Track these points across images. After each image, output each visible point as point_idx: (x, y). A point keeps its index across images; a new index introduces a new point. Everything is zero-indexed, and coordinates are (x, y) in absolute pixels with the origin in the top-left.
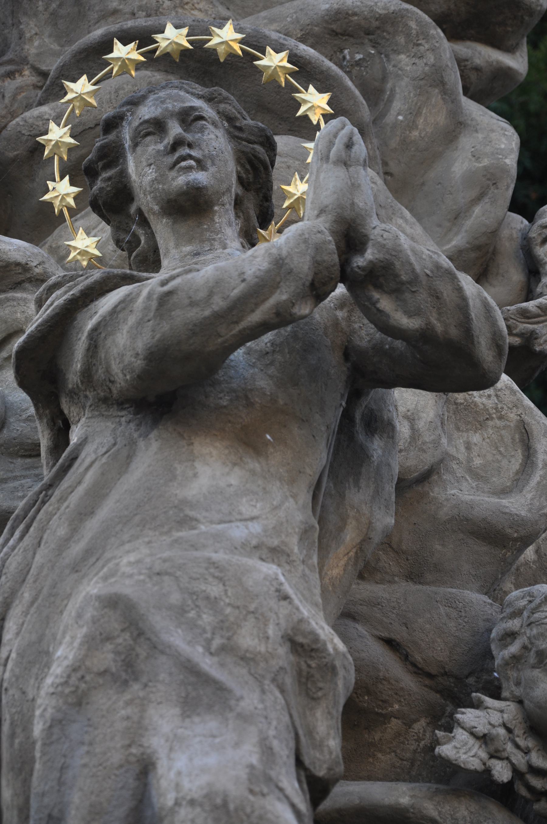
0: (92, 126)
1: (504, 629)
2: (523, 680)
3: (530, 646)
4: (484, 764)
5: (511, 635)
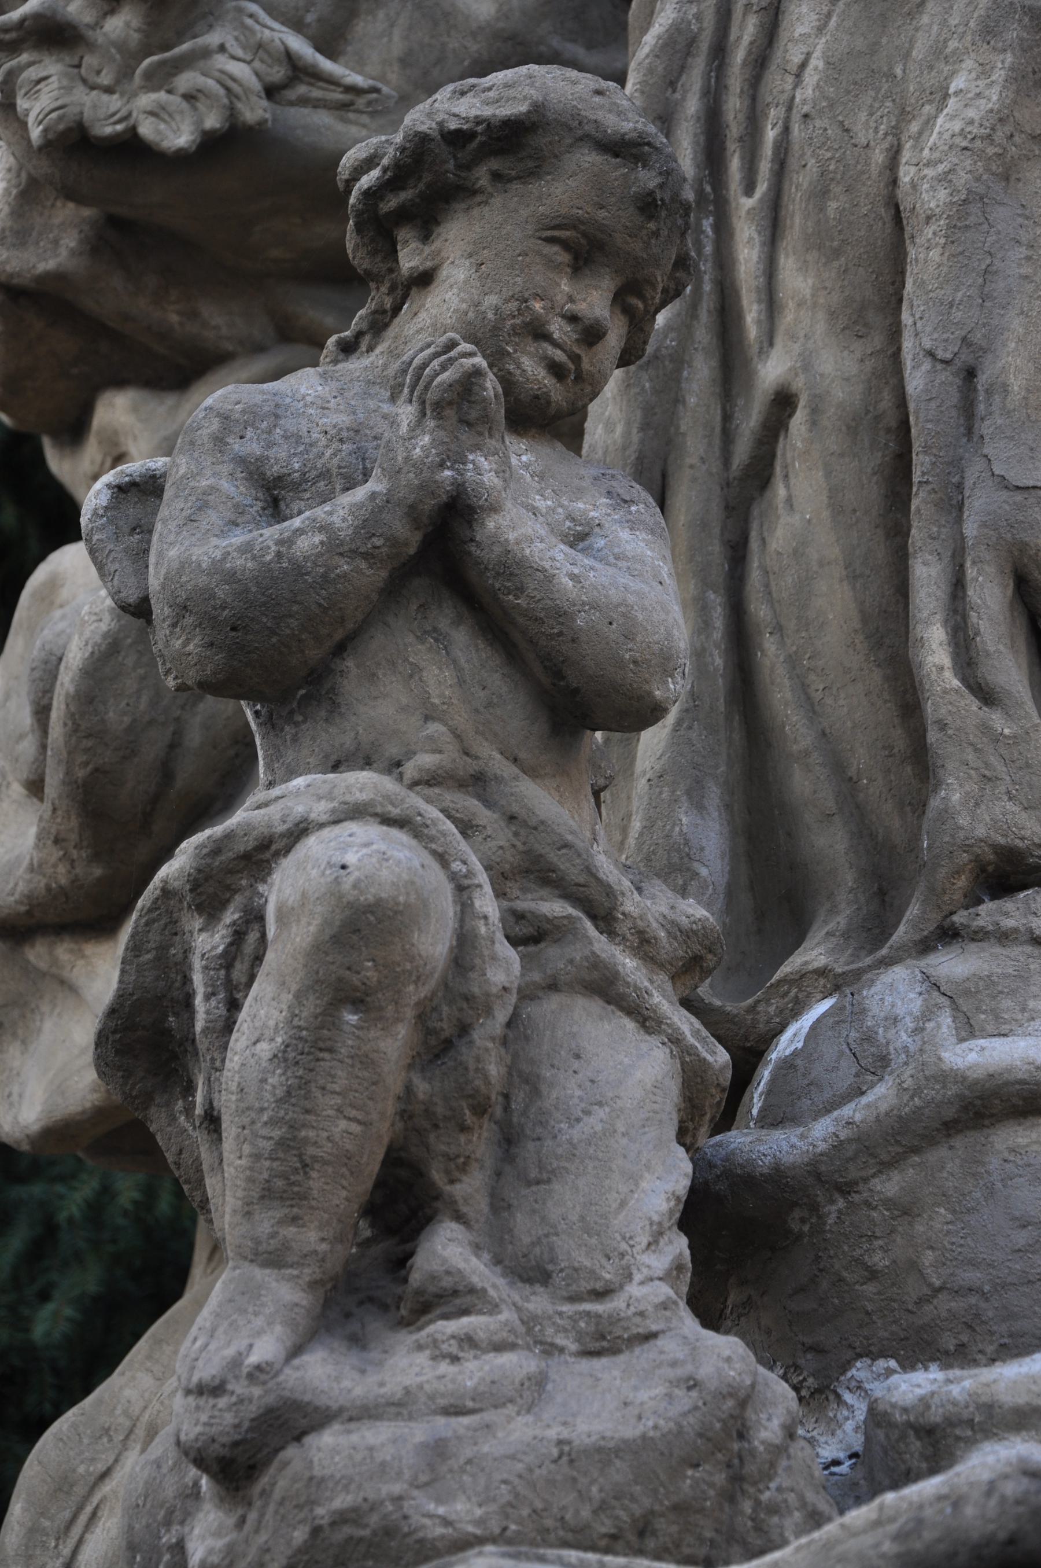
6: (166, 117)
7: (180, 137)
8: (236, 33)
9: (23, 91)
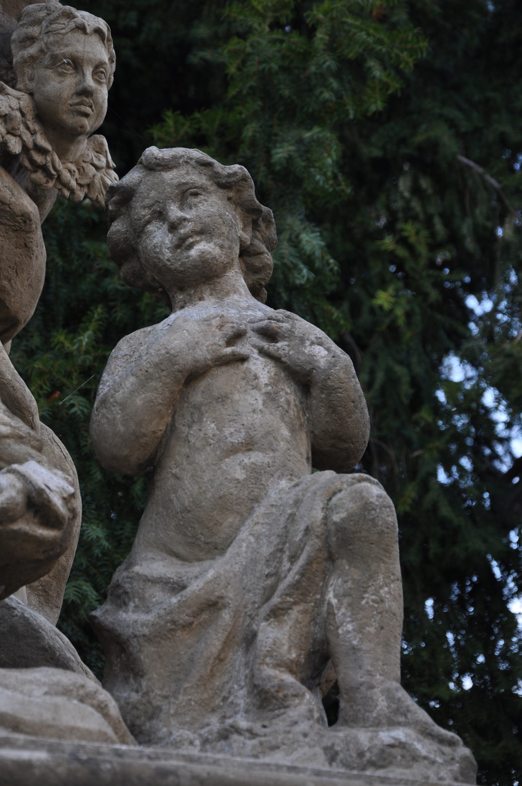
1: (26, 34)
2: (36, 77)
3: (46, 50)
4: (3, 137)
5: (31, 39)
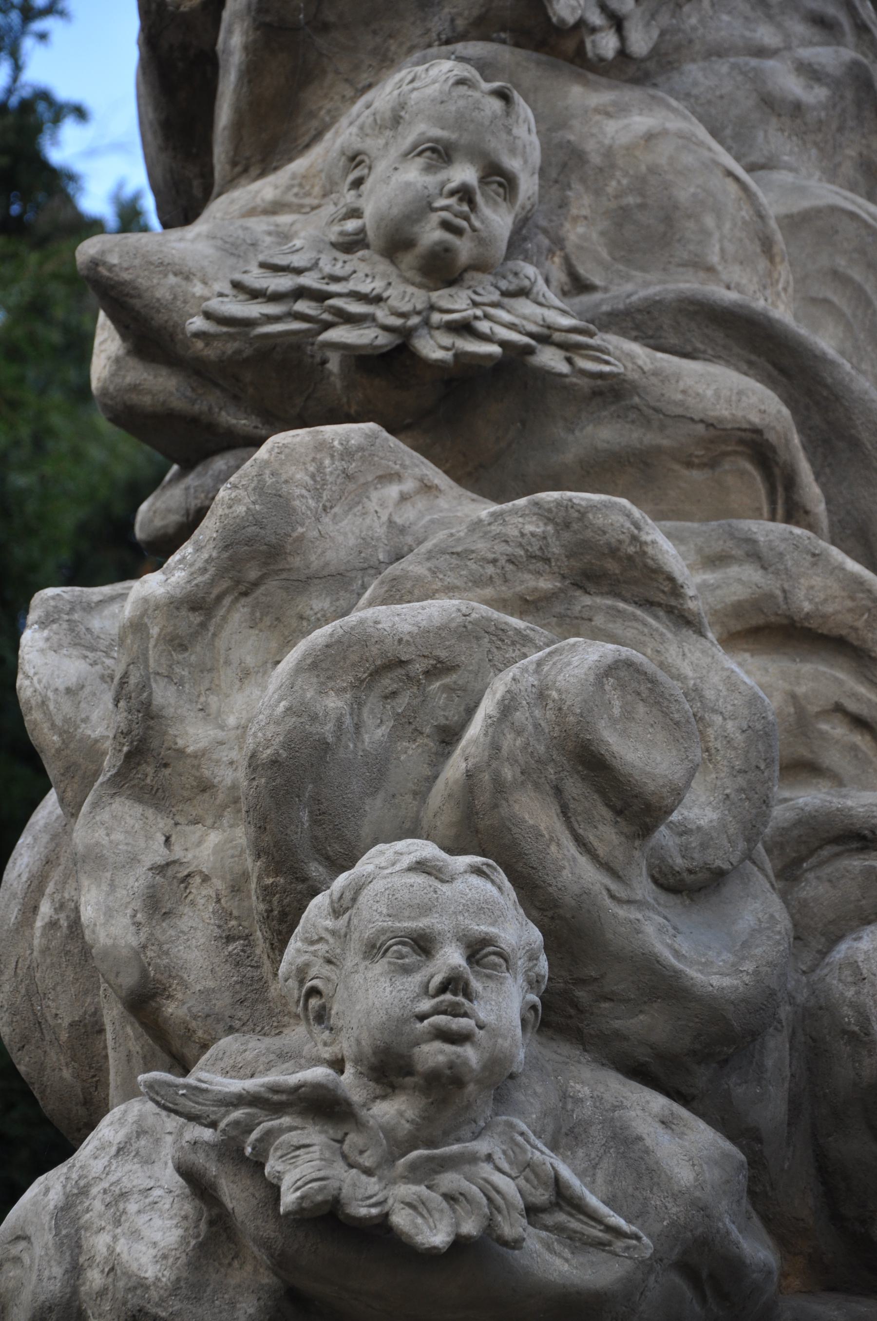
0: (696, 418)
6: (425, 1212)
7: (436, 1236)
8: (504, 1147)
9: (279, 1153)
